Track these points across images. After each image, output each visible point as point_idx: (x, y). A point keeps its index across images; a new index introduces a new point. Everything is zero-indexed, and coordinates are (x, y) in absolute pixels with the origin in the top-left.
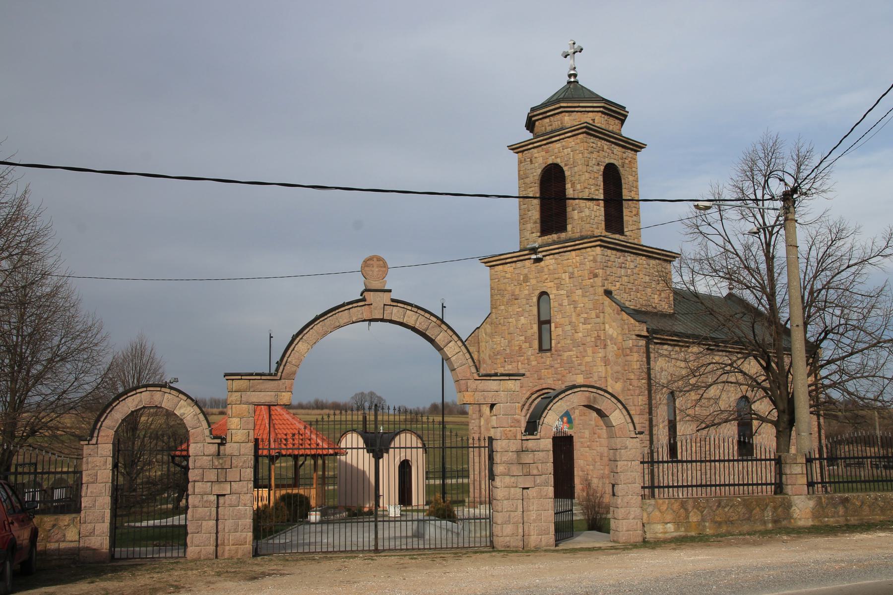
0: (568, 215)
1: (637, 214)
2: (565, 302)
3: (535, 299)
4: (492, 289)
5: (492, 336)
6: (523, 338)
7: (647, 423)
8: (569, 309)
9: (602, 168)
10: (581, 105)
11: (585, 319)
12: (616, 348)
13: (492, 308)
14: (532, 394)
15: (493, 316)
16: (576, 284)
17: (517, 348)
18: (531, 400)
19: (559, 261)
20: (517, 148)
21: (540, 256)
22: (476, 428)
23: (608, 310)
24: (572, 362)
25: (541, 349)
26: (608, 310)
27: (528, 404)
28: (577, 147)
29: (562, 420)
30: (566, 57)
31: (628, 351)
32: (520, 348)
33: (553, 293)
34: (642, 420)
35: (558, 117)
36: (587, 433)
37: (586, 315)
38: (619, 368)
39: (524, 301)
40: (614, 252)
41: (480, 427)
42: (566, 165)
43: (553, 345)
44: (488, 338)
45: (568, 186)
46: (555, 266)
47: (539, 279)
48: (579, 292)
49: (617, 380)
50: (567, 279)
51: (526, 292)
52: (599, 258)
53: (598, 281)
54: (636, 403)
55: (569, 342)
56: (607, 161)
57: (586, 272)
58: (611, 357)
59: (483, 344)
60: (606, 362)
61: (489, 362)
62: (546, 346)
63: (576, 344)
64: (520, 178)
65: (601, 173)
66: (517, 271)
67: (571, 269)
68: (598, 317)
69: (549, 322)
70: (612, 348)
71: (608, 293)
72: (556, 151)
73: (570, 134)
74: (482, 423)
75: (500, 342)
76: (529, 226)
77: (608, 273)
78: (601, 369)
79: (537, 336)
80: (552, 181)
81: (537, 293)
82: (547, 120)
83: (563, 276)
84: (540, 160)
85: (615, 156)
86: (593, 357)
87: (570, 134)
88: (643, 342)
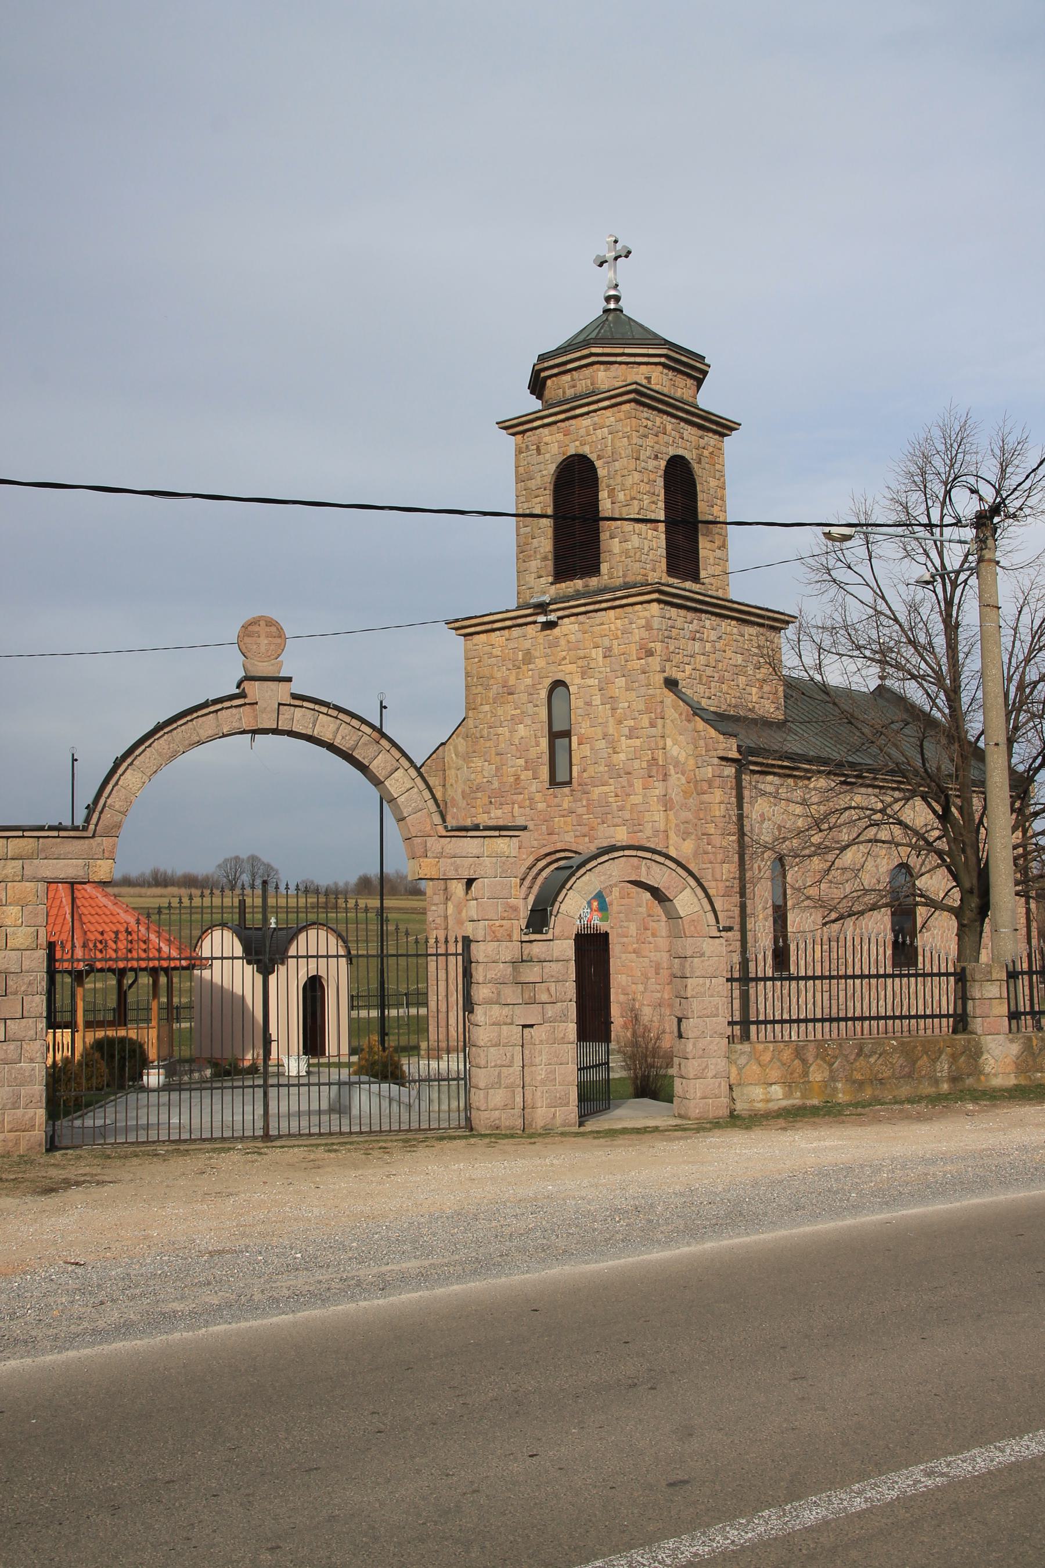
0: (603, 546)
2: (597, 700)
3: (543, 694)
5: (467, 758)
6: (521, 762)
8: (603, 711)
10: (627, 351)
11: (631, 729)
12: (683, 780)
13: (468, 709)
14: (538, 860)
15: (470, 722)
16: (616, 667)
17: (512, 779)
18: (535, 870)
19: (586, 627)
20: (514, 427)
21: (552, 617)
22: (438, 921)
23: (671, 713)
24: (608, 804)
25: (553, 782)
26: (671, 713)
27: (530, 878)
30: (601, 265)
32: (518, 779)
33: (575, 683)
35: (587, 372)
36: (633, 929)
37: (632, 723)
38: (689, 815)
39: (524, 697)
40: (682, 612)
41: (446, 917)
42: (599, 458)
43: (575, 774)
44: (461, 762)
45: (603, 495)
46: (580, 635)
47: (551, 659)
48: (621, 682)
49: (685, 835)
50: (600, 659)
51: (529, 681)
52: (656, 623)
53: (655, 662)
54: (718, 877)
55: (602, 769)
57: (634, 648)
58: (675, 795)
59: (451, 773)
60: (667, 804)
61: (462, 803)
62: (561, 777)
64: (519, 479)
65: (661, 473)
67: (606, 642)
68: (653, 725)
69: (567, 734)
70: (676, 779)
71: (671, 684)
72: (582, 432)
74: (450, 911)
75: (483, 769)
76: (534, 564)
79: (546, 758)
80: (575, 488)
82: (567, 378)
84: (554, 448)
85: (686, 442)
86: (645, 796)
88: (730, 771)
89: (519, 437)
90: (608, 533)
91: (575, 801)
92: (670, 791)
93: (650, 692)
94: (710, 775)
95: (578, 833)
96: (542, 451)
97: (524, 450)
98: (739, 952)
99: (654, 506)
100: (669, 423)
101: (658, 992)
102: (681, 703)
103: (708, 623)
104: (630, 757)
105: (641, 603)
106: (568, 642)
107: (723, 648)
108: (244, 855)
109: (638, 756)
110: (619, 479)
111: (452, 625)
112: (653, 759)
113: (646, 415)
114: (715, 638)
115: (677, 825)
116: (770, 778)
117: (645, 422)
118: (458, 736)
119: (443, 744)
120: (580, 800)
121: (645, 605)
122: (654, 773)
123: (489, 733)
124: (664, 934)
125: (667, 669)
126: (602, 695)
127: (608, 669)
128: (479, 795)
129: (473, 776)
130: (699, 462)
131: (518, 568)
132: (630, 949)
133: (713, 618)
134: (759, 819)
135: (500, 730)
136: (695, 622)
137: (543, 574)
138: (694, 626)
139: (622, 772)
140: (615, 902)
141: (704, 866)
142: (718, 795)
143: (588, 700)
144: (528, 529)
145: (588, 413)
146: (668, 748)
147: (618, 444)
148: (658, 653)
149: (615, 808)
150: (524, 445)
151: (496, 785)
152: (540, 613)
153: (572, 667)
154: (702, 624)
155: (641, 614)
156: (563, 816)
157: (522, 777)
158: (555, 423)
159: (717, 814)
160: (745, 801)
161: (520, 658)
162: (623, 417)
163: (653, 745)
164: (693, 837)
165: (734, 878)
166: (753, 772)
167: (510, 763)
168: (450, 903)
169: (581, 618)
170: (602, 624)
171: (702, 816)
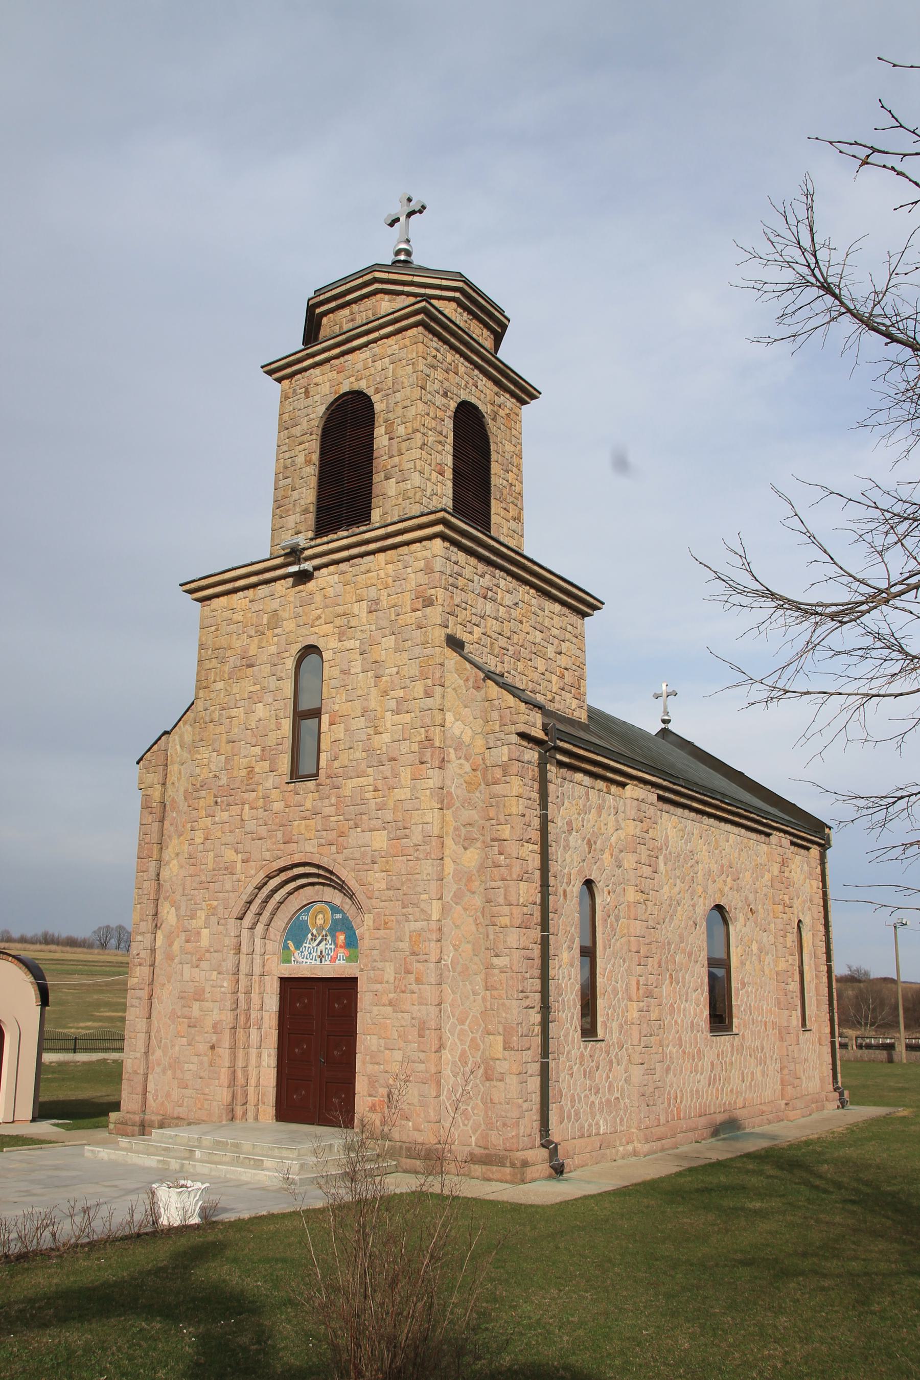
0: (376, 490)
1: (518, 519)
2: (357, 667)
3: (290, 664)
4: (202, 647)
5: (193, 748)
6: (257, 750)
7: (536, 952)
8: (364, 680)
9: (453, 405)
10: (416, 279)
11: (400, 701)
12: (467, 767)
13: (198, 688)
14: (270, 877)
15: (200, 705)
16: (384, 623)
17: (244, 773)
20: (279, 371)
21: (307, 566)
22: (143, 954)
23: (453, 679)
24: (364, 801)
25: (296, 775)
26: (453, 679)
27: (258, 901)
28: (403, 353)
29: (335, 942)
30: (391, 225)
31: (498, 773)
32: (251, 770)
33: (329, 646)
34: (524, 942)
35: (368, 303)
36: (389, 972)
37: (401, 693)
38: (474, 815)
39: (266, 669)
40: (473, 561)
41: (153, 950)
42: (377, 391)
43: (323, 763)
44: (186, 755)
46: (340, 588)
47: (301, 621)
48: (390, 641)
49: (467, 843)
50: (364, 614)
51: (273, 649)
52: (438, 564)
53: (435, 614)
54: (513, 899)
55: (359, 754)
56: (464, 396)
57: (408, 597)
58: (456, 788)
59: (173, 769)
60: (444, 800)
61: (183, 806)
62: (307, 767)
63: (376, 759)
65: (450, 413)
66: (256, 606)
67: (373, 593)
69: (316, 713)
70: (458, 767)
71: (455, 643)
72: (360, 366)
73: (390, 329)
74: (159, 943)
76: (291, 520)
77: (457, 600)
78: (433, 817)
79: (288, 744)
80: (348, 432)
81: (296, 648)
82: (346, 312)
83: (356, 608)
84: (325, 389)
85: (483, 394)
86: (413, 788)
87: (390, 329)
88: (532, 755)
89: (286, 382)
90: (382, 474)
91: (321, 798)
92: (448, 782)
93: (428, 652)
94: (505, 759)
95: (323, 841)
96: (311, 393)
97: (290, 395)
98: (537, 1008)
99: (440, 448)
100: (463, 367)
101: (422, 1062)
102: (468, 665)
103: (502, 583)
104: (396, 737)
105: (420, 540)
106: (325, 597)
107: (520, 617)
108: (114, 924)
109: (407, 736)
110: (399, 411)
111: (188, 587)
112: (428, 739)
113: (435, 345)
114: (511, 604)
115: (456, 829)
116: (579, 776)
117: (434, 353)
118: (185, 723)
119: (166, 733)
120: (328, 797)
121: (424, 543)
122: (427, 757)
123: (221, 715)
124: (433, 981)
125: (451, 625)
126: (364, 659)
127: (373, 627)
128: (203, 793)
129: (198, 770)
130: (494, 419)
131: (273, 525)
132: (385, 1000)
133: (509, 579)
134: (566, 828)
135: (234, 712)
136: (487, 576)
137: (302, 529)
138: (487, 581)
139: (384, 758)
140: (367, 936)
141: (494, 884)
142: (515, 785)
143: (345, 668)
144: (289, 480)
145: (366, 345)
146: (448, 724)
147: (400, 372)
148: (440, 601)
149: (374, 807)
150: (291, 390)
151: (224, 780)
152: (294, 566)
153: (328, 628)
154: (495, 581)
155: (419, 555)
156: (305, 819)
157: (257, 770)
158: (328, 360)
159: (514, 810)
160: (550, 799)
161: (265, 621)
162: (408, 344)
163: (428, 721)
164: (479, 844)
165: (535, 904)
166: (561, 764)
167: (243, 752)
168: (159, 933)
169: (343, 566)
170: (368, 571)
171: (492, 815)
